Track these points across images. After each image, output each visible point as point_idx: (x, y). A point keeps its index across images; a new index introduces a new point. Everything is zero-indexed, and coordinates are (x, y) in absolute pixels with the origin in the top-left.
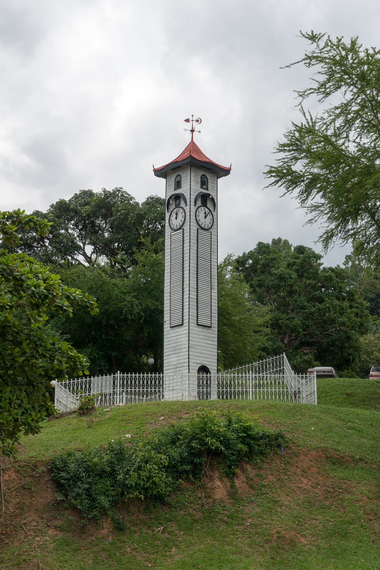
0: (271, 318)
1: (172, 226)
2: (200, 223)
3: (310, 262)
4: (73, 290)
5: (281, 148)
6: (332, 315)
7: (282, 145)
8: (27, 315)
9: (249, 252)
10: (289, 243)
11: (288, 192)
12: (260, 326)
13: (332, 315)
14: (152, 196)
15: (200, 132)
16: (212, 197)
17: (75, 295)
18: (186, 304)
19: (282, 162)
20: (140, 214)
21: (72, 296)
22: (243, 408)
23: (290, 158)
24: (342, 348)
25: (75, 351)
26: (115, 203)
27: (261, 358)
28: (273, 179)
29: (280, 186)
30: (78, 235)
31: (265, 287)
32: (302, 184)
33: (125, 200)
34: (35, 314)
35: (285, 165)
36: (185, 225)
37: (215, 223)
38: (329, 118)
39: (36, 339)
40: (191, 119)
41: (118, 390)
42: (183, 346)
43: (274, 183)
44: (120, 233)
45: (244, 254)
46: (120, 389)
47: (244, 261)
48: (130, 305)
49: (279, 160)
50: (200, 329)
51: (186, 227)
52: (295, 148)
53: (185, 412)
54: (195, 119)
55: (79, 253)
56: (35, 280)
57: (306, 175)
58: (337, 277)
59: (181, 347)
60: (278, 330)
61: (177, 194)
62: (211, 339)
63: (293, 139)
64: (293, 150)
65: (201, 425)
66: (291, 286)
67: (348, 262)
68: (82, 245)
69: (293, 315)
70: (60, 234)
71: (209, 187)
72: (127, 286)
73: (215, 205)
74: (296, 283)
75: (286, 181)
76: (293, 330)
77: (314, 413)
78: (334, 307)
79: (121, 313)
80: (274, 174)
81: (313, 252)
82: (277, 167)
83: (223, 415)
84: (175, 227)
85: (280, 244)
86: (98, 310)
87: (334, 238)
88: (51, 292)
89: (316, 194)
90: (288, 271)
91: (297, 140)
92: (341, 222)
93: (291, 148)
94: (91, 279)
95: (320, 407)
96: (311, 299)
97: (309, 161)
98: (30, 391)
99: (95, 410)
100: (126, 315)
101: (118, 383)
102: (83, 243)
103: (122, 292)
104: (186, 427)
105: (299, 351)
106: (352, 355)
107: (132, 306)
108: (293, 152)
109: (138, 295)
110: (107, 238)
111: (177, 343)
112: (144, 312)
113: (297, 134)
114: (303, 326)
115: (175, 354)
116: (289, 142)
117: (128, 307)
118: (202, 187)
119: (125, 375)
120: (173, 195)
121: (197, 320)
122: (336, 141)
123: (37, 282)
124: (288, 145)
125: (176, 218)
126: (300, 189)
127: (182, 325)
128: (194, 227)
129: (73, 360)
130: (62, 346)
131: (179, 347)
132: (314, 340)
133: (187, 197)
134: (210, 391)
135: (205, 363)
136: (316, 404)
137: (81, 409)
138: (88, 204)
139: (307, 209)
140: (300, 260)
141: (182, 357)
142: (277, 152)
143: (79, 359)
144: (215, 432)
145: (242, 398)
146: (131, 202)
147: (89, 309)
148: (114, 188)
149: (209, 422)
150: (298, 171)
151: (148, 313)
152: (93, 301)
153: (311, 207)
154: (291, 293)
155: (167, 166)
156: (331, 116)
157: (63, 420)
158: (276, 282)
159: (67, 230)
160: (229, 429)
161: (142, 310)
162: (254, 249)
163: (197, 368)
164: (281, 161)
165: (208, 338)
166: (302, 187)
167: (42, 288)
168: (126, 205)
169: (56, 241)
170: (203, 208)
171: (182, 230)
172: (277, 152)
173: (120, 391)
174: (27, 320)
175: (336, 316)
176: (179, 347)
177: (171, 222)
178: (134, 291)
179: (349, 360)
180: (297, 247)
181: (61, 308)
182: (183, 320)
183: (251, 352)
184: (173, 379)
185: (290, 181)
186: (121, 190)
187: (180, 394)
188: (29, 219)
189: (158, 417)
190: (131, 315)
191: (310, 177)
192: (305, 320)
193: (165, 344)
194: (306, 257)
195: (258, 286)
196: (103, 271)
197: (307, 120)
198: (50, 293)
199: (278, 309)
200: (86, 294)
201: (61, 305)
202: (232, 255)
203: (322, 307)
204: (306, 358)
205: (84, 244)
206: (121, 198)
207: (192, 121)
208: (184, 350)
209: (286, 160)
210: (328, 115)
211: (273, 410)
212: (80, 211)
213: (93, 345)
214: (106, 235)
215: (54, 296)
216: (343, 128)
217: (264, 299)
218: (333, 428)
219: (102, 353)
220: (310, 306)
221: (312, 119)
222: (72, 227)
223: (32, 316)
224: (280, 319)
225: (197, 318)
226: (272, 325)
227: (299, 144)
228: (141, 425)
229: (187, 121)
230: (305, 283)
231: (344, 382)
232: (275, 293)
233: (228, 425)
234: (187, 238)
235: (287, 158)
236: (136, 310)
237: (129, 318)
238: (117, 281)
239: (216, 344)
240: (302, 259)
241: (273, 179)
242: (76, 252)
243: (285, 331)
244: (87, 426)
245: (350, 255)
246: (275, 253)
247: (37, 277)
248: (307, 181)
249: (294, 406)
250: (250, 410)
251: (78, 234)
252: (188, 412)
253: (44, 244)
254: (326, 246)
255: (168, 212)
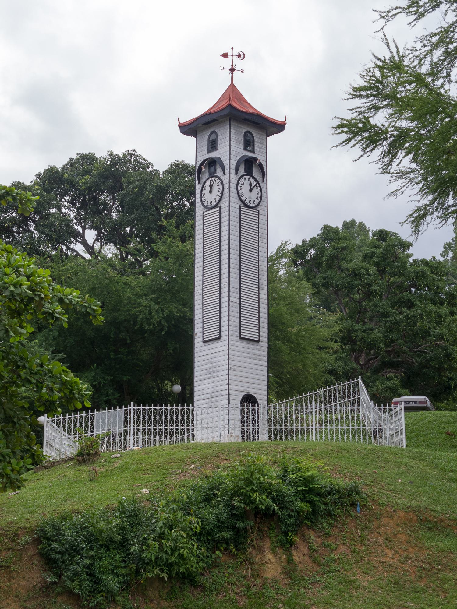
0: (340, 328)
1: (205, 203)
2: (243, 199)
3: (395, 252)
4: (68, 290)
5: (355, 93)
6: (426, 325)
7: (356, 88)
8: (5, 325)
9: (311, 239)
10: (365, 226)
11: (365, 154)
12: (327, 340)
13: (426, 325)
14: (176, 162)
15: (242, 71)
16: (260, 162)
17: (70, 297)
18: (225, 309)
19: (356, 112)
20: (160, 186)
21: (67, 299)
22: (303, 452)
23: (367, 107)
24: (440, 370)
25: (72, 375)
26: (126, 171)
27: (327, 383)
28: (345, 137)
29: (354, 146)
30: (75, 216)
31: (333, 287)
32: (385, 143)
33: (139, 168)
34: (16, 324)
35: (360, 116)
36: (223, 200)
37: (264, 199)
38: (423, 50)
39: (17, 358)
40: (230, 54)
41: (132, 428)
42: (220, 368)
43: (345, 141)
44: (133, 213)
45: (304, 242)
46: (134, 426)
47: (304, 252)
48: (147, 312)
49: (353, 109)
50: (244, 344)
51: (224, 205)
52: (374, 93)
53: (224, 457)
54: (235, 52)
55: (77, 241)
56: (15, 276)
57: (389, 130)
58: (432, 273)
59: (218, 369)
60: (352, 345)
61: (212, 159)
62: (258, 357)
63: (373, 80)
64: (372, 95)
65: (246, 476)
66: (369, 285)
67: (448, 253)
68: (80, 229)
69: (372, 325)
70: (49, 214)
71: (255, 148)
72: (144, 287)
73: (263, 173)
74: (375, 281)
75: (362, 139)
76: (372, 346)
77: (401, 460)
78: (429, 314)
79: (135, 323)
80: (345, 129)
81: (399, 239)
82: (349, 119)
83: (276, 462)
84: (209, 204)
85: (354, 228)
86: (102, 318)
87: (428, 218)
88: (37, 293)
89: (403, 157)
90: (364, 265)
91: (378, 81)
92: (438, 195)
93: (369, 92)
94: (93, 276)
95: (410, 451)
96: (396, 302)
97: (395, 111)
98: (8, 431)
99: (100, 456)
100: (141, 325)
101: (132, 418)
102: (82, 227)
103: (136, 295)
104: (226, 479)
105: (380, 374)
106: (453, 380)
107: (150, 313)
108: (372, 98)
109: (158, 298)
110: (116, 220)
111: (212, 363)
112: (167, 321)
113: (378, 74)
114: (386, 340)
115: (210, 378)
116: (366, 84)
117: (145, 314)
118: (245, 149)
119: (141, 408)
120: (206, 160)
121: (240, 332)
122: (434, 81)
123: (18, 279)
124: (365, 89)
125: (211, 192)
126: (381, 150)
127: (219, 338)
128: (236, 204)
129: (69, 386)
130: (53, 367)
131: (215, 369)
132: (400, 359)
133: (226, 163)
134: (258, 429)
135: (252, 391)
136: (405, 447)
137: (80, 454)
138: (88, 172)
139: (390, 175)
140: (381, 250)
141: (219, 383)
142: (350, 98)
143: (78, 385)
144: (265, 484)
145: (303, 438)
146: (148, 170)
147: (91, 317)
148: (124, 151)
149: (257, 471)
150: (379, 125)
151: (173, 323)
152: (96, 305)
153: (397, 173)
154: (369, 295)
155: (197, 119)
156: (425, 46)
157: (56, 471)
158: (348, 280)
159: (59, 208)
160: (285, 481)
161: (164, 318)
162: (318, 235)
163: (240, 398)
164: (355, 110)
165: (255, 356)
166: (385, 147)
167: (25, 287)
168: (141, 174)
169: (44, 223)
170: (247, 178)
171: (218, 209)
172: (350, 98)
173: (134, 429)
174: (3, 331)
175: (431, 326)
176: (215, 369)
177: (203, 198)
178: (154, 292)
179: (449, 387)
180: (376, 231)
181: (52, 315)
182: (220, 332)
183: (314, 376)
184: (207, 413)
185: (367, 138)
186: (134, 153)
187: (217, 434)
188: (5, 192)
189: (186, 465)
190: (149, 325)
191: (395, 133)
192: (387, 331)
193: (196, 364)
194: (389, 246)
195: (323, 285)
196: (110, 266)
197: (392, 52)
198: (36, 295)
199: (351, 317)
200: (87, 296)
201: (51, 311)
202: (287, 243)
203: (412, 314)
204: (390, 383)
205: (84, 228)
206: (134, 165)
207: (232, 55)
208: (221, 373)
209: (363, 109)
210: (421, 44)
211: (345, 454)
212: (78, 182)
213: (97, 368)
214: (114, 215)
215: (42, 299)
216: (442, 64)
217: (331, 303)
218: (428, 480)
219: (109, 378)
220: (395, 313)
221: (398, 52)
222: (67, 205)
223: (11, 327)
224: (353, 330)
225: (240, 329)
226: (343, 339)
227: (381, 87)
228: (163, 476)
229: (225, 55)
230: (388, 282)
231: (443, 416)
232: (347, 295)
233: (283, 476)
234: (225, 219)
235: (364, 107)
236: (156, 318)
237: (146, 329)
238: (130, 279)
239: (266, 364)
240: (384, 248)
241: (345, 137)
242: (72, 239)
243: (360, 346)
244: (88, 479)
245: (450, 243)
246: (346, 239)
247: (17, 272)
248: (391, 139)
249: (374, 450)
250: (312, 455)
251: (75, 214)
252: (227, 458)
253: (28, 228)
254: (416, 230)
255: (199, 183)
